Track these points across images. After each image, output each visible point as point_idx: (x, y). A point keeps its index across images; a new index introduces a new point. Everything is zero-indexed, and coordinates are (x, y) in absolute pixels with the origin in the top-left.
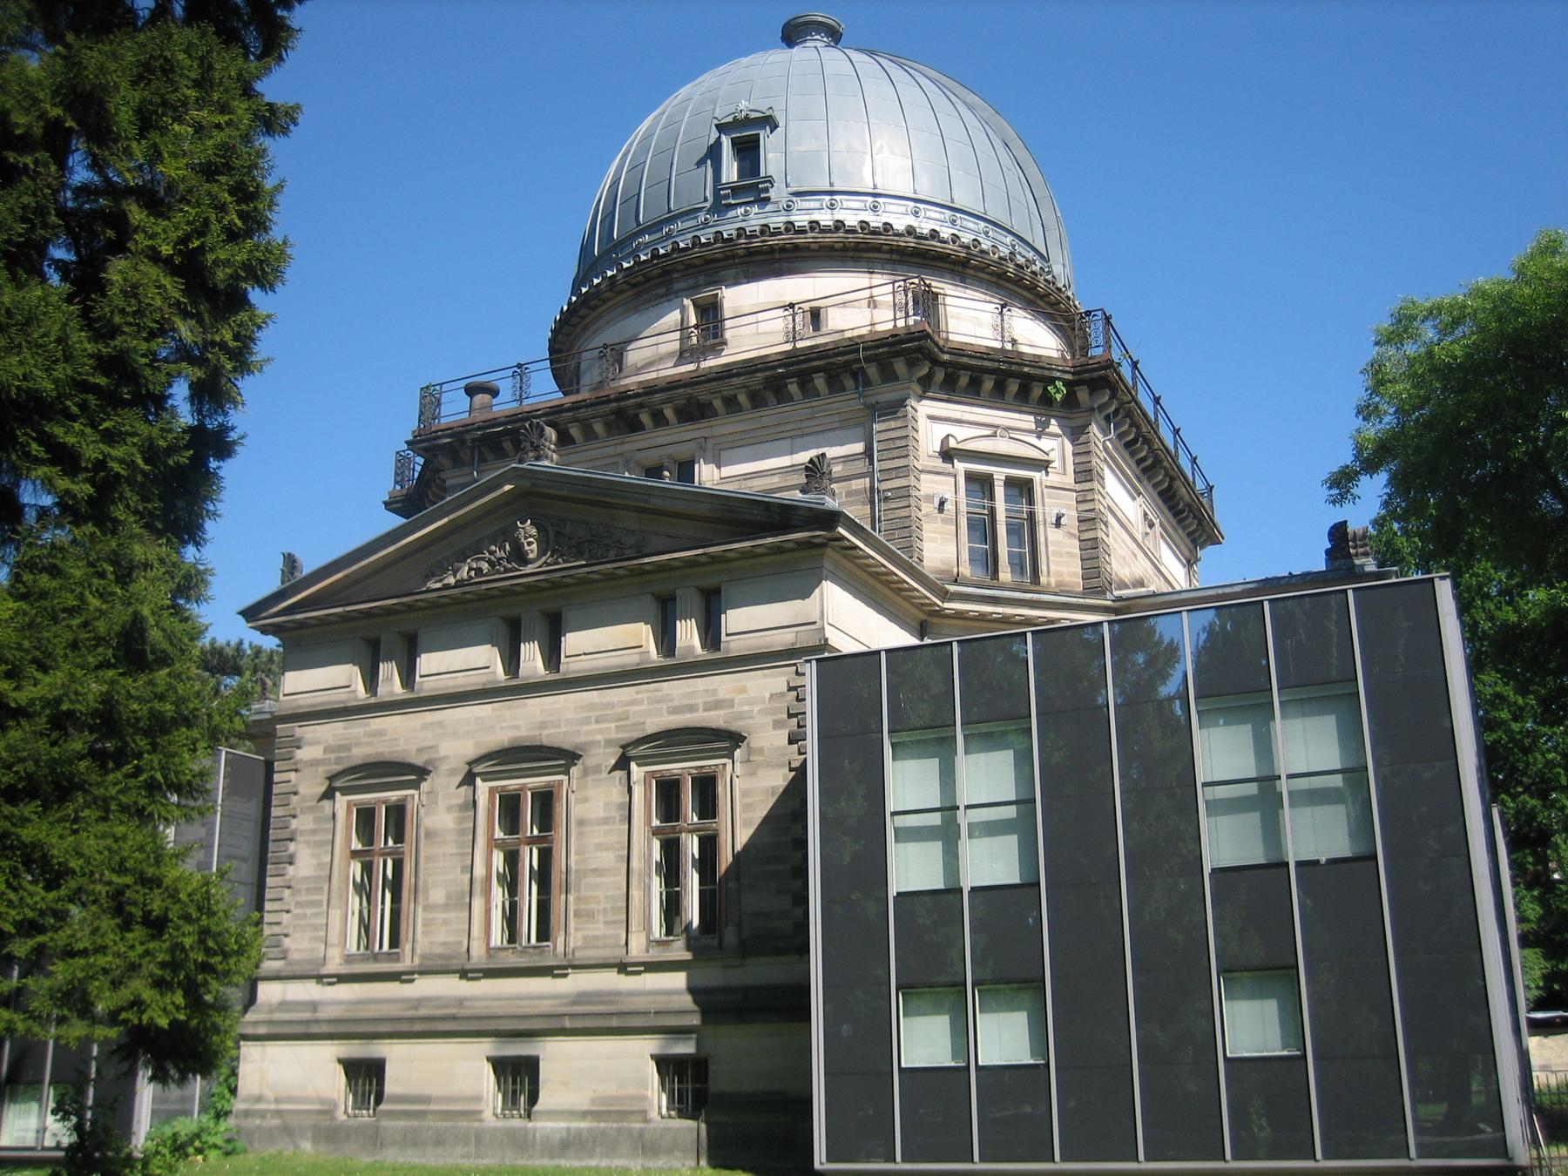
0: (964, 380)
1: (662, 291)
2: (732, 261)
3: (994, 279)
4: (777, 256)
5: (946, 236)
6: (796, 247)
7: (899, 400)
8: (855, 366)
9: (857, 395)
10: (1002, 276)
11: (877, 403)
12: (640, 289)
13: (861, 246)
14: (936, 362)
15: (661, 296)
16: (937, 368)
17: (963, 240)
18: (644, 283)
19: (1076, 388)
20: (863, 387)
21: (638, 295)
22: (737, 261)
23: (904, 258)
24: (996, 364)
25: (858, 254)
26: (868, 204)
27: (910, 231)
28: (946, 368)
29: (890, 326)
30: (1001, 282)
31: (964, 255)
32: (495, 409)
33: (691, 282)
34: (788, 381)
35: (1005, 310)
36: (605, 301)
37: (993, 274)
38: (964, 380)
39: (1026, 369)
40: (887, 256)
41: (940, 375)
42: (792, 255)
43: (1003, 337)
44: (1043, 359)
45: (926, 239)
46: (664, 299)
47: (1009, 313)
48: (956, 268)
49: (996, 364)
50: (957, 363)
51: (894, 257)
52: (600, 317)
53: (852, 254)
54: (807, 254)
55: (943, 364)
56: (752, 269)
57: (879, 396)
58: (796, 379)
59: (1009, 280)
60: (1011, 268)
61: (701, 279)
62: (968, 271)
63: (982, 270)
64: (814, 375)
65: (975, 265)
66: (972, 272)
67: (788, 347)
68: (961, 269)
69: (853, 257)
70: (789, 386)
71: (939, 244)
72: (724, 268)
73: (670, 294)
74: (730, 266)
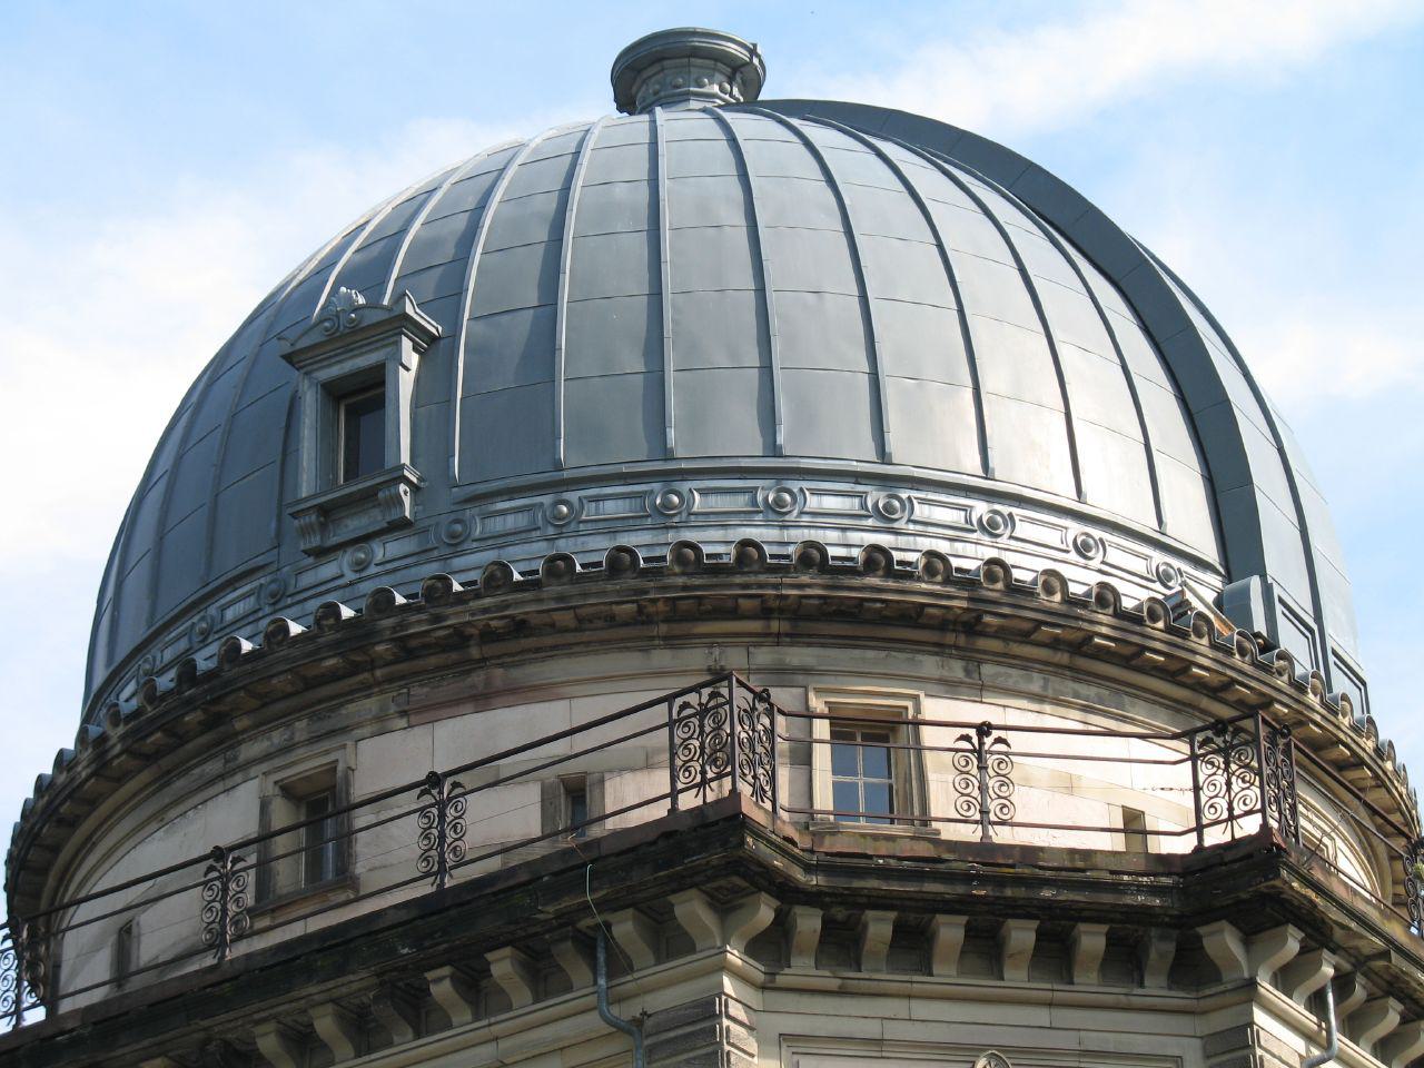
0: (879, 928)
1: (213, 767)
2: (365, 676)
3: (1062, 657)
4: (475, 652)
5: (1027, 577)
6: (520, 627)
7: (696, 1004)
8: (585, 923)
9: (592, 1000)
10: (1082, 646)
11: (644, 1013)
12: (165, 762)
13: (683, 605)
14: (788, 895)
15: (212, 782)
16: (798, 910)
17: (1016, 574)
18: (172, 749)
19: (1202, 930)
20: (610, 977)
21: (164, 781)
22: (378, 673)
23: (804, 626)
24: (960, 889)
25: (678, 629)
26: (1100, 556)
27: (877, 559)
28: (822, 906)
29: (660, 811)
30: (1082, 662)
31: (964, 604)
32: (1334, 879)
33: (278, 737)
34: (430, 975)
35: (988, 741)
36: (93, 803)
37: (1055, 644)
38: (879, 928)
39: (1047, 893)
40: (755, 626)
41: (809, 923)
42: (512, 646)
43: (984, 812)
44: (1098, 860)
45: (853, 572)
46: (220, 787)
47: (1001, 747)
48: (950, 638)
49: (960, 889)
50: (855, 892)
51: (775, 626)
52: (89, 844)
53: (663, 628)
54: (548, 641)
55: (812, 898)
56: (419, 692)
57: (649, 998)
58: (446, 970)
59: (1102, 654)
60: (1104, 623)
61: (301, 728)
62: (982, 643)
63: (1025, 637)
64: (489, 956)
65: (1002, 628)
66: (995, 645)
67: (425, 888)
68: (962, 640)
69: (665, 638)
70: (434, 989)
71: (891, 584)
72: (350, 695)
73: (232, 772)
74: (365, 690)
